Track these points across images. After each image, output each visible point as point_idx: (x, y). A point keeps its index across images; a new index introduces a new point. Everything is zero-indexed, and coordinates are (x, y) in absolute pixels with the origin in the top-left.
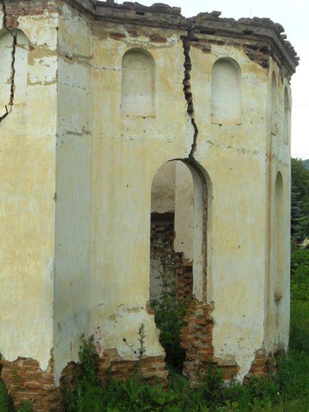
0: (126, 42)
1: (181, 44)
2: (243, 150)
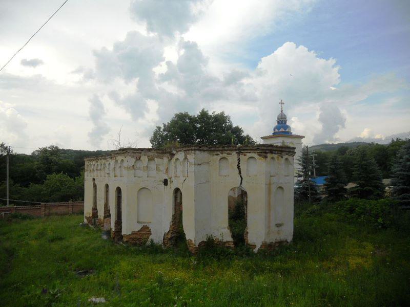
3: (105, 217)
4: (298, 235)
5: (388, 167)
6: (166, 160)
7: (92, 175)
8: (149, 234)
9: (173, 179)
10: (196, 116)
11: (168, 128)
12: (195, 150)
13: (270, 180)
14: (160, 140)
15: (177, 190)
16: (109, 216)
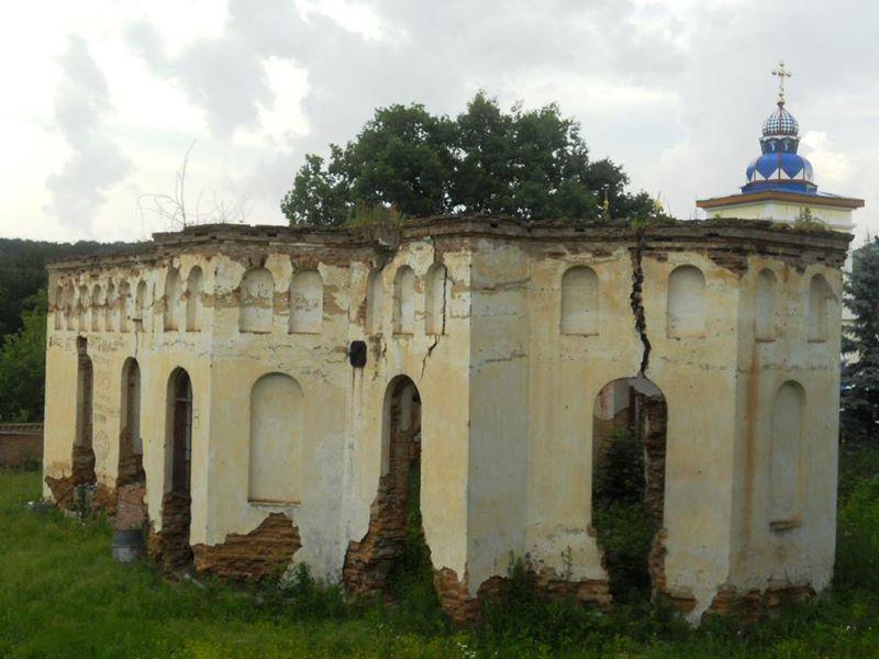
1: (629, 256)
2: (707, 366)
3: (122, 482)
4: (850, 568)
6: (359, 272)
7: (75, 322)
8: (289, 545)
9: (388, 342)
10: (454, 119)
11: (347, 162)
12: (474, 235)
13: (754, 357)
14: (319, 205)
15: (402, 388)
16: (140, 476)
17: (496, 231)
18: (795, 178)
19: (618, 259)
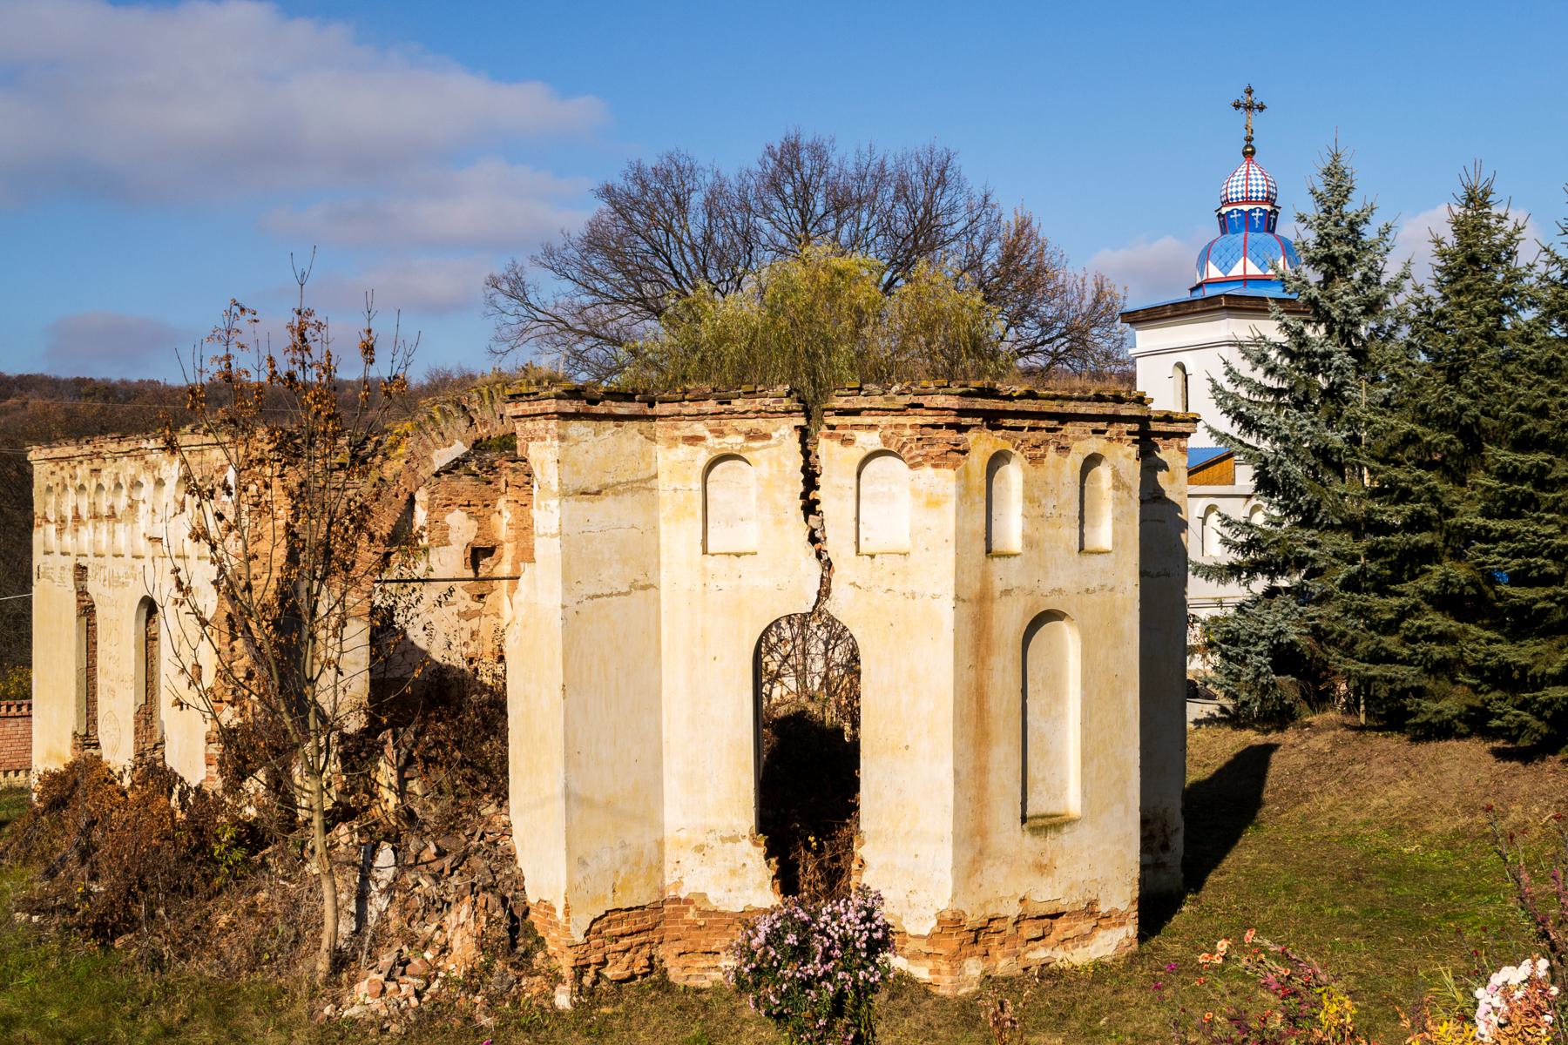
0: (707, 448)
5: (454, 691)
17: (600, 409)
18: (1231, 274)
19: (780, 443)
